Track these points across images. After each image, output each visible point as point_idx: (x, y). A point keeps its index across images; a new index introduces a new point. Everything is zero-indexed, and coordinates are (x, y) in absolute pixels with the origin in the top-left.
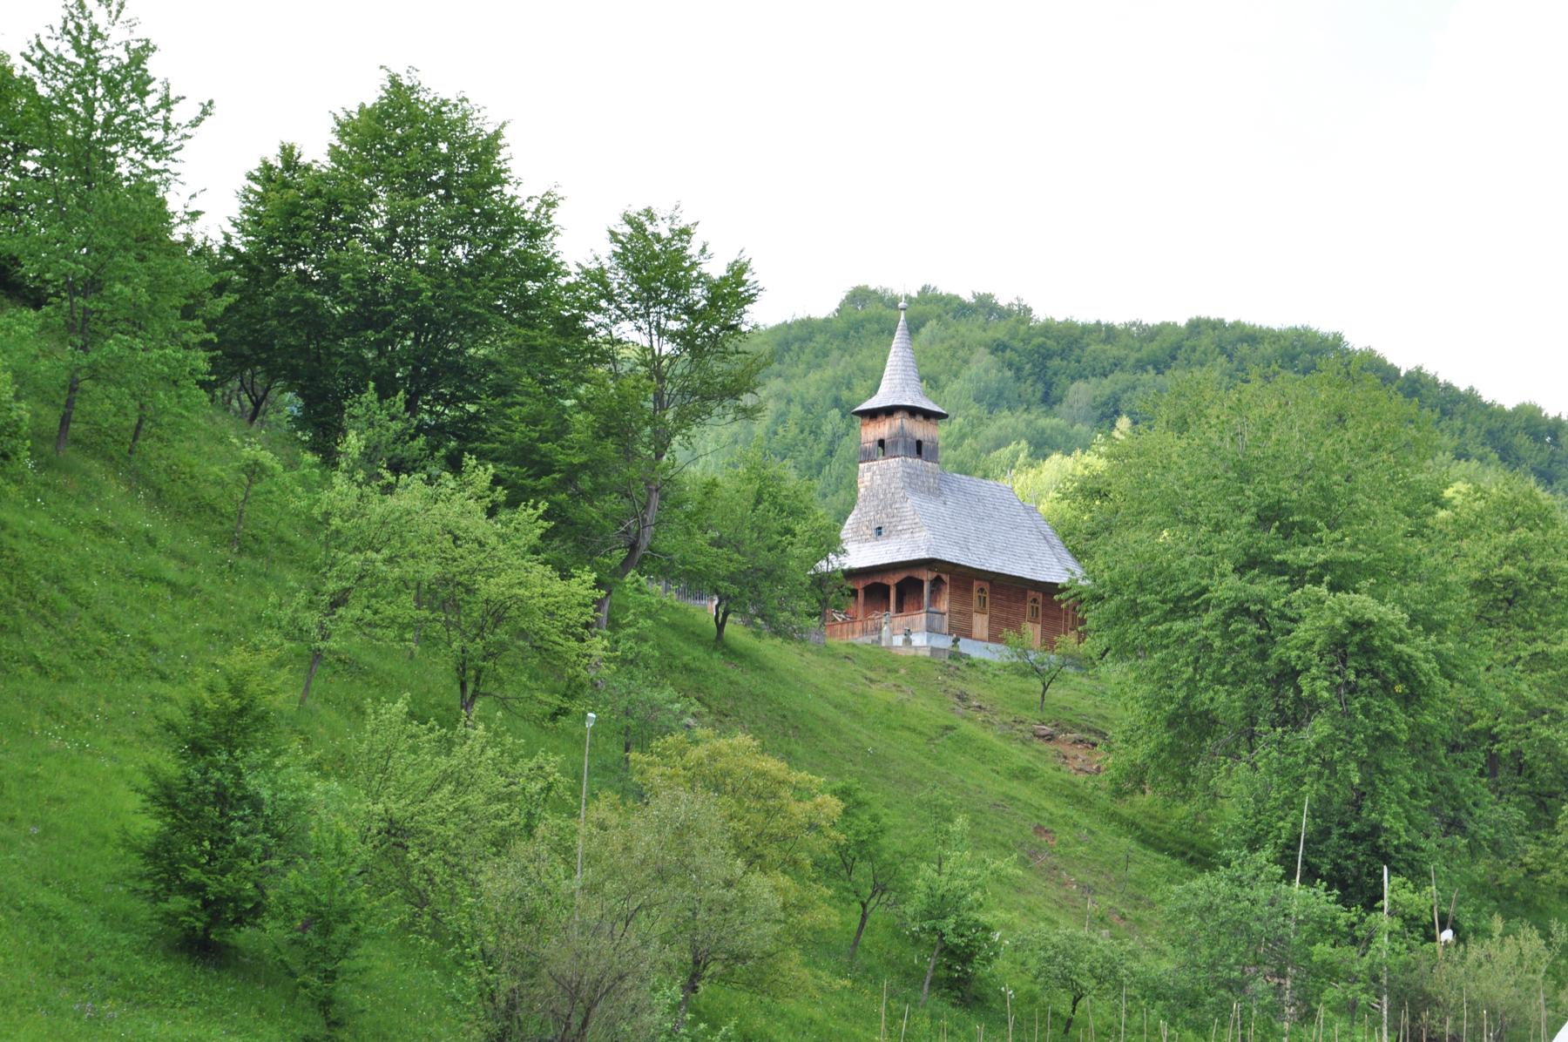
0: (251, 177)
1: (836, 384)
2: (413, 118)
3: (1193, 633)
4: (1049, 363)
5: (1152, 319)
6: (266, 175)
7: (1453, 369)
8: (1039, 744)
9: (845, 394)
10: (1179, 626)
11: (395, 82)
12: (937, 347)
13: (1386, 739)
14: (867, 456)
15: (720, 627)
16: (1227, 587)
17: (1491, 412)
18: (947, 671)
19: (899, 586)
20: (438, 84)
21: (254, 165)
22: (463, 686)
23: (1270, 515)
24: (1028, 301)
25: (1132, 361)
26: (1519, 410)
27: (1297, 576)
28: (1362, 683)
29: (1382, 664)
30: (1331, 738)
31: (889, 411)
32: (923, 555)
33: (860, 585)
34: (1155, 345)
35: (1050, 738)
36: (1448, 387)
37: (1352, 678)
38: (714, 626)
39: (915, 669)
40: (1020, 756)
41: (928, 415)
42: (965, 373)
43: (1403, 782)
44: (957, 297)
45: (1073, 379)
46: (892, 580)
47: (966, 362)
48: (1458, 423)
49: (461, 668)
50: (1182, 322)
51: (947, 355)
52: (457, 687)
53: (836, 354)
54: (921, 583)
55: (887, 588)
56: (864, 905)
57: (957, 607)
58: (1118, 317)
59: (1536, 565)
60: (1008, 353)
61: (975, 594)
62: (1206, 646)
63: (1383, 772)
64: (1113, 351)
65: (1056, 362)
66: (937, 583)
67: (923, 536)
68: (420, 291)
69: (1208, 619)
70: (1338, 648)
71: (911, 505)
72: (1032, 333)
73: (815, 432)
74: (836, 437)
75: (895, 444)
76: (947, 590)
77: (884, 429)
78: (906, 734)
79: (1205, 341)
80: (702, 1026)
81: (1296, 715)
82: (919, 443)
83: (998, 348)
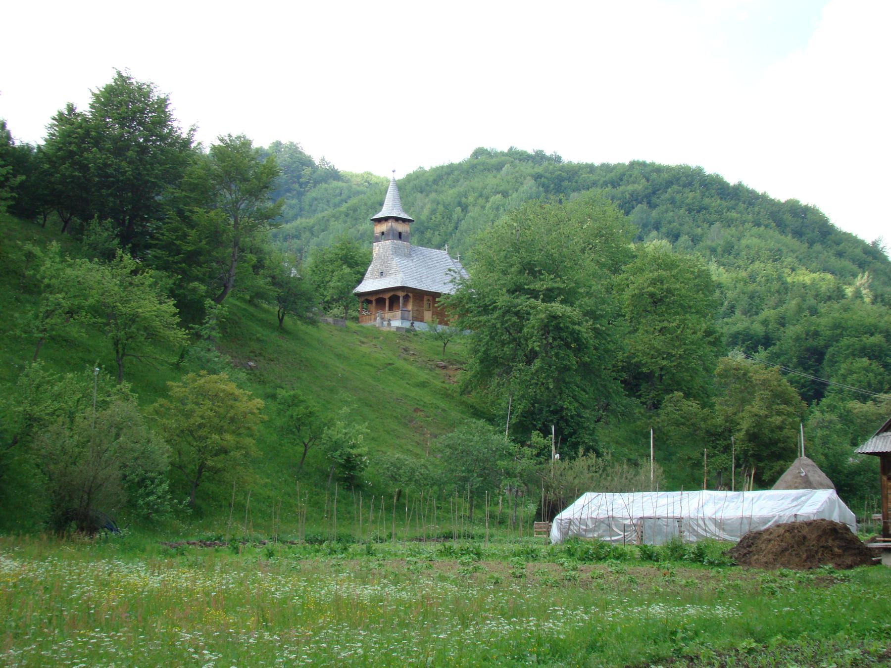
0: (54, 119)
1: (460, 195)
2: (130, 92)
3: (489, 321)
4: (563, 184)
5: (613, 161)
6: (61, 119)
7: (757, 184)
8: (438, 371)
9: (464, 200)
10: (483, 318)
11: (120, 75)
12: (509, 177)
13: (567, 369)
14: (377, 240)
15: (281, 320)
16: (503, 300)
17: (773, 203)
18: (402, 338)
19: (390, 298)
20: (139, 76)
21: (55, 114)
22: (117, 352)
23: (529, 268)
24: (559, 154)
25: (601, 182)
26: (787, 202)
27: (534, 294)
28: (556, 343)
29: (564, 335)
30: (542, 368)
31: (386, 219)
32: (399, 285)
33: (373, 299)
34: (612, 174)
35: (445, 367)
36: (753, 192)
37: (551, 341)
38: (278, 321)
39: (388, 339)
40: (423, 376)
41: (404, 221)
42: (521, 189)
43: (574, 387)
44: (526, 152)
45: (574, 191)
46: (387, 296)
47: (522, 184)
48: (757, 209)
49: (116, 344)
50: (627, 163)
51: (513, 181)
52: (115, 353)
53: (462, 180)
54: (399, 297)
55: (384, 300)
56: (306, 446)
57: (415, 308)
58: (597, 161)
59: (665, 287)
60: (543, 180)
61: (425, 302)
62: (494, 326)
63: (564, 382)
64: (593, 177)
65: (566, 183)
66: (406, 298)
67: (400, 276)
68: (127, 171)
69: (495, 315)
70: (545, 329)
71: (396, 262)
72: (562, 169)
73: (450, 218)
74: (459, 220)
75: (388, 234)
76: (411, 301)
77: (383, 227)
78: (368, 368)
79: (636, 172)
80: (176, 501)
81: (531, 357)
82: (400, 234)
83: (537, 177)
